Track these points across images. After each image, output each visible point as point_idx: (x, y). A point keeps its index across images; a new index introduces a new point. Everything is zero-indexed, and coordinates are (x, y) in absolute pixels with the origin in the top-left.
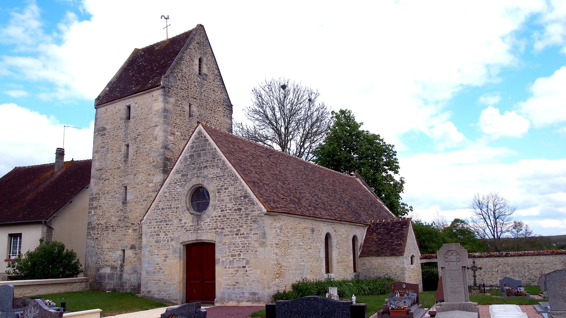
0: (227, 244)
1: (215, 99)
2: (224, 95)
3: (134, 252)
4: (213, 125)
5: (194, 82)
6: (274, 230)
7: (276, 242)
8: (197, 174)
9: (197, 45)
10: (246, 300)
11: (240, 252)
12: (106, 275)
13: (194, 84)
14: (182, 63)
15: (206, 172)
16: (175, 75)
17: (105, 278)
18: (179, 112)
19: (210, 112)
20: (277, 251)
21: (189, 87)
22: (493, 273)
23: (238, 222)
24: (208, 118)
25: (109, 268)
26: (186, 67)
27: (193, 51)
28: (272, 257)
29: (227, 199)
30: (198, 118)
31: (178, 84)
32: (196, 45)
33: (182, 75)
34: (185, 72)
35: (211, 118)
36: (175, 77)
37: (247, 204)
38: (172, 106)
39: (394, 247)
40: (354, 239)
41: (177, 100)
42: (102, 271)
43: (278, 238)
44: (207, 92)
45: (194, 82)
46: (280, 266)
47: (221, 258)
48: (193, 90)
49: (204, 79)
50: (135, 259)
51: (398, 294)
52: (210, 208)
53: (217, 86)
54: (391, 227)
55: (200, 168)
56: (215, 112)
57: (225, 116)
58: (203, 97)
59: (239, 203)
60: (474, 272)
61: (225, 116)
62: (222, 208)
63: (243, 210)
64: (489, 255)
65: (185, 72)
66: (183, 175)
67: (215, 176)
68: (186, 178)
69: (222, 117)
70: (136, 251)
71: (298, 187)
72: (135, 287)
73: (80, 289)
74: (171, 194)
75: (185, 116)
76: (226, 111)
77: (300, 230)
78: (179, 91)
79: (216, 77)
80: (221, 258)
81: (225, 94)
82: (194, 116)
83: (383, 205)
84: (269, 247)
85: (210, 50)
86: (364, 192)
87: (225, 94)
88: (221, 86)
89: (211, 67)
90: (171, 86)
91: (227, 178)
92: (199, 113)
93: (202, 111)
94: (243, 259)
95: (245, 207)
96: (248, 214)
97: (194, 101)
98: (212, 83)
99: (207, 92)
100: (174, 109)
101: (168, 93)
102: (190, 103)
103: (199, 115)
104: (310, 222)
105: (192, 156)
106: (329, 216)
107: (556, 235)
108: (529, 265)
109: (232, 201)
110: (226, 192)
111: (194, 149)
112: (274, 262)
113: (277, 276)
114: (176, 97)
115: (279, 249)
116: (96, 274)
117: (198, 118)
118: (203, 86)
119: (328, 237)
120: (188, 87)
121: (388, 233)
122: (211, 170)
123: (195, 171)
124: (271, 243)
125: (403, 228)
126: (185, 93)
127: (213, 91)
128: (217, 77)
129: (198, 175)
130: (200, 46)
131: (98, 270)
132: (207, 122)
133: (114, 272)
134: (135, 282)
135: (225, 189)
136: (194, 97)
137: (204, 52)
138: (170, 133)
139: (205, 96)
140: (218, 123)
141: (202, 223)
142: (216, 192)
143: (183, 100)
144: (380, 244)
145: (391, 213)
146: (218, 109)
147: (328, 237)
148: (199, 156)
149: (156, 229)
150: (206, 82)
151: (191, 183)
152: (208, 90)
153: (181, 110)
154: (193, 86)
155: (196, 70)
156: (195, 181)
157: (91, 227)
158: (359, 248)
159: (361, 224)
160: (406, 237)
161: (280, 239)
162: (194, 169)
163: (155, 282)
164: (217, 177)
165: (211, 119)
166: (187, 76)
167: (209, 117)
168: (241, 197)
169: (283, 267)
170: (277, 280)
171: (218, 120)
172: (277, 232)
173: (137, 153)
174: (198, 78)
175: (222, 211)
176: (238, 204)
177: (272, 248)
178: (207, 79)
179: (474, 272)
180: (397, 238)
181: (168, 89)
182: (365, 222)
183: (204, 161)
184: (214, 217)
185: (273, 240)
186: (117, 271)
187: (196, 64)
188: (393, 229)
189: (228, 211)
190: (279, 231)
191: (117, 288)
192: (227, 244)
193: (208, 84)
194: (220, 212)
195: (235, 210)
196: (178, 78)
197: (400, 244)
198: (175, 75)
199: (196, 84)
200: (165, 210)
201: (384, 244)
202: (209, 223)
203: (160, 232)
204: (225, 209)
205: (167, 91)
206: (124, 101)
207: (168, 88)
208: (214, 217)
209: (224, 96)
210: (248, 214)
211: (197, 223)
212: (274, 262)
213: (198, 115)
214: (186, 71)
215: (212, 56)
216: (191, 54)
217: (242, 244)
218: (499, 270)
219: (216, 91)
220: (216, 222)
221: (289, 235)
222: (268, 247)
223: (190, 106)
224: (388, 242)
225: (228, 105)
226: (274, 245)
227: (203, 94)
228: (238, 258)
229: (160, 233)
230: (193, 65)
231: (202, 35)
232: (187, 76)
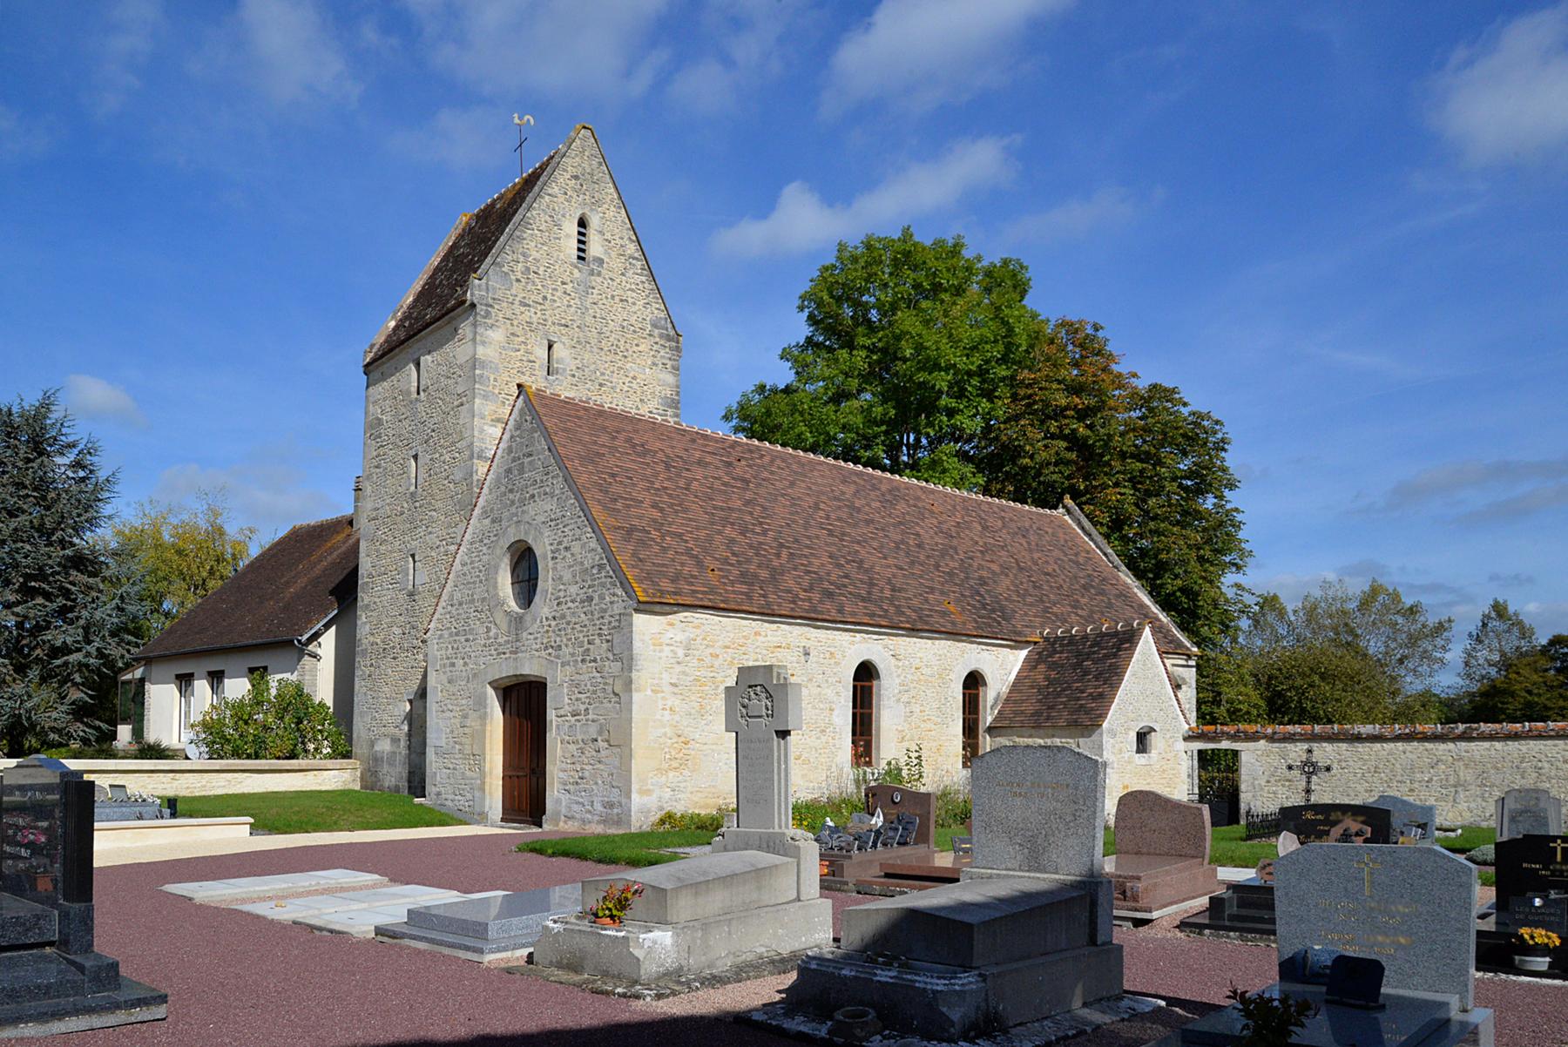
0: (565, 685)
1: (625, 324)
2: (657, 309)
4: (618, 390)
5: (563, 283)
6: (667, 649)
7: (672, 681)
9: (574, 181)
10: (596, 818)
13: (561, 289)
14: (525, 235)
15: (531, 509)
16: (505, 269)
17: (383, 761)
18: (519, 364)
19: (609, 358)
20: (676, 702)
21: (549, 296)
22: (1416, 785)
24: (603, 374)
26: (539, 246)
27: (561, 198)
28: (658, 717)
30: (574, 376)
31: (514, 292)
32: (568, 182)
33: (528, 269)
34: (534, 259)
35: (613, 372)
36: (506, 274)
37: (603, 585)
38: (496, 351)
39: (1083, 702)
40: (974, 681)
41: (513, 334)
43: (678, 668)
44: (603, 307)
45: (563, 283)
46: (682, 739)
48: (559, 305)
49: (592, 273)
51: (878, 817)
53: (633, 287)
54: (1091, 646)
55: (523, 502)
56: (626, 357)
57: (656, 365)
58: (589, 320)
59: (589, 582)
60: (1309, 778)
61: (656, 365)
64: (1407, 731)
65: (534, 259)
66: (493, 521)
69: (647, 370)
71: (797, 541)
73: (340, 784)
75: (536, 372)
76: (662, 353)
77: (757, 650)
78: (518, 309)
79: (630, 264)
81: (657, 306)
82: (560, 371)
83: (1136, 590)
84: (649, 692)
85: (613, 190)
86: (1076, 555)
87: (657, 306)
88: (646, 285)
89: (617, 237)
90: (494, 299)
92: (578, 361)
93: (587, 356)
94: (593, 721)
96: (605, 611)
97: (564, 332)
98: (618, 281)
99: (603, 307)
100: (504, 356)
101: (485, 317)
102: (551, 338)
103: (578, 368)
104: (797, 630)
105: (509, 471)
106: (872, 615)
108: (1540, 764)
112: (663, 730)
113: (675, 764)
114: (509, 326)
115: (681, 697)
117: (574, 376)
118: (590, 291)
119: (866, 673)
120: (545, 298)
121: (1079, 664)
123: (513, 510)
124: (655, 682)
125: (1119, 649)
126: (536, 313)
127: (622, 300)
128: (634, 262)
130: (582, 185)
132: (601, 385)
135: (567, 549)
136: (563, 322)
137: (593, 200)
138: (492, 420)
139: (595, 317)
140: (634, 386)
141: (525, 634)
143: (529, 333)
144: (1049, 693)
145: (1156, 611)
146: (635, 349)
147: (866, 673)
148: (521, 471)
149: (450, 650)
150: (599, 279)
152: (605, 301)
153: (524, 358)
154: (559, 294)
155: (568, 251)
158: (989, 705)
159: (997, 638)
160: (1121, 676)
161: (684, 673)
165: (615, 375)
166: (542, 269)
167: (608, 372)
168: (593, 567)
169: (692, 742)
170: (671, 774)
171: (634, 378)
172: (676, 654)
173: (430, 476)
174: (576, 271)
175: (558, 604)
177: (660, 695)
178: (604, 272)
179: (1309, 778)
180: (1097, 678)
181: (484, 308)
182: (1019, 634)
185: (664, 676)
187: (568, 236)
188: (1094, 653)
189: (570, 604)
190: (681, 652)
192: (565, 685)
193: (606, 285)
196: (513, 278)
197: (1101, 695)
198: (505, 269)
199: (569, 287)
201: (1059, 695)
203: (456, 658)
204: (564, 600)
205: (482, 313)
206: (410, 350)
207: (486, 305)
209: (656, 312)
210: (605, 611)
212: (663, 730)
213: (574, 368)
214: (537, 256)
215: (620, 208)
216: (554, 210)
218: (1435, 778)
219: (630, 300)
221: (716, 664)
222: (646, 690)
223: (550, 347)
224: (1069, 688)
225: (668, 335)
226: (668, 689)
227: (591, 311)
230: (559, 239)
231: (586, 153)
232: (542, 269)
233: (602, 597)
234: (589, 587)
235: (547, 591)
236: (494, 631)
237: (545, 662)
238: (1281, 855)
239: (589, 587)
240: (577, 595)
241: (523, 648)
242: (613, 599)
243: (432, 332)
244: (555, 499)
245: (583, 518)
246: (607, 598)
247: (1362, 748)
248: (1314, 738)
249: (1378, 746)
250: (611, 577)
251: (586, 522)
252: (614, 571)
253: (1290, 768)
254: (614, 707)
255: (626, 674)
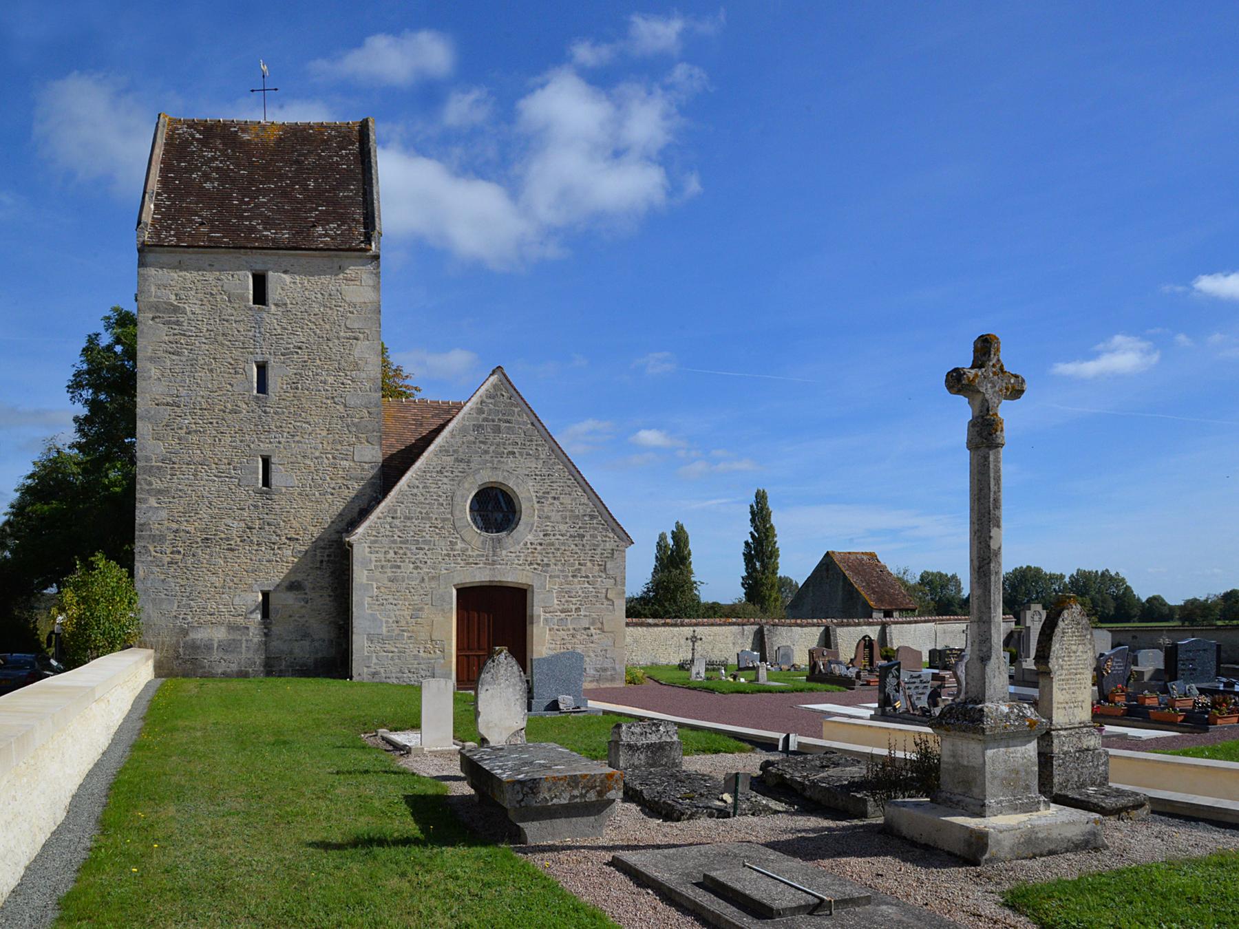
0: (554, 591)
3: (299, 596)
8: (492, 462)
11: (580, 605)
12: (213, 644)
23: (576, 556)
25: (223, 629)
29: (556, 516)
37: (595, 529)
42: (199, 635)
47: (542, 613)
50: (303, 611)
52: (521, 527)
59: (580, 525)
62: (547, 530)
63: (588, 537)
67: (533, 474)
68: (465, 467)
70: (306, 594)
72: (306, 666)
74: (429, 492)
80: (542, 613)
91: (558, 480)
94: (585, 616)
95: (592, 533)
107: (809, 575)
109: (568, 520)
110: (553, 503)
111: (484, 416)
116: (178, 643)
122: (522, 460)
129: (495, 466)
131: (185, 632)
133: (239, 638)
134: (307, 656)
141: (504, 552)
142: (535, 503)
151: (477, 477)
156: (486, 477)
157: (150, 535)
162: (486, 452)
163: (391, 655)
164: (536, 475)
176: (578, 527)
183: (507, 442)
184: (529, 544)
186: (248, 635)
191: (250, 670)
192: (554, 591)
194: (542, 537)
195: (571, 536)
200: (414, 520)
202: (518, 554)
208: (529, 544)
211: (493, 551)
217: (583, 592)
220: (532, 553)
228: (576, 614)
229: (402, 564)
233: (593, 536)
234: (580, 528)
235: (533, 525)
236: (460, 545)
237: (531, 574)
238: (589, 701)
239: (580, 528)
240: (567, 531)
241: (502, 562)
242: (604, 539)
243: (292, 255)
244: (541, 461)
245: (573, 481)
246: (599, 538)
247: (651, 629)
248: (696, 625)
249: (656, 629)
250: (603, 525)
251: (576, 484)
252: (606, 521)
253: (701, 639)
254: (608, 609)
255: (619, 587)
